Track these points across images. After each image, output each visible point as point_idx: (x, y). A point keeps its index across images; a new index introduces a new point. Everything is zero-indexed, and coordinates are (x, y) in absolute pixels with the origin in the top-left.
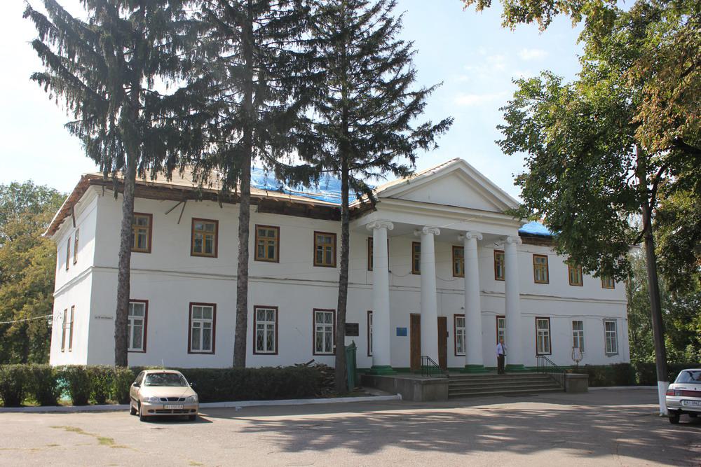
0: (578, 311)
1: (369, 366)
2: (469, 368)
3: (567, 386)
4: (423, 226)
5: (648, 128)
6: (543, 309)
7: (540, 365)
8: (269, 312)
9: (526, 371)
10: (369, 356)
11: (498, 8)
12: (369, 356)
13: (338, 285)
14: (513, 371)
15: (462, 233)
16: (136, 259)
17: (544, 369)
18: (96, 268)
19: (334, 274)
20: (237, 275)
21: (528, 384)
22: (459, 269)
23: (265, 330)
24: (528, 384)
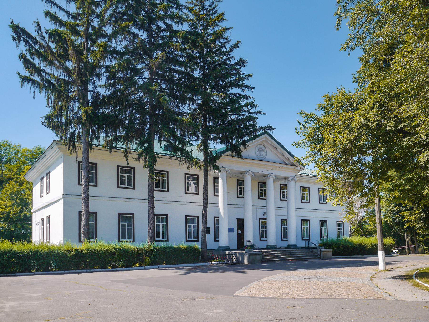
0: (323, 216)
1: (216, 247)
2: (289, 247)
3: (322, 255)
4: (289, 177)
5: (379, 130)
6: (306, 215)
7: (307, 245)
8: (163, 218)
9: (299, 248)
10: (215, 241)
11: (44, 1)
12: (215, 241)
13: (202, 204)
14: (291, 248)
15: (265, 176)
16: (157, 195)
17: (309, 248)
18: (66, 195)
19: (200, 198)
20: (202, 202)
21: (302, 254)
22: (240, 192)
23: (192, 229)
24: (302, 254)
